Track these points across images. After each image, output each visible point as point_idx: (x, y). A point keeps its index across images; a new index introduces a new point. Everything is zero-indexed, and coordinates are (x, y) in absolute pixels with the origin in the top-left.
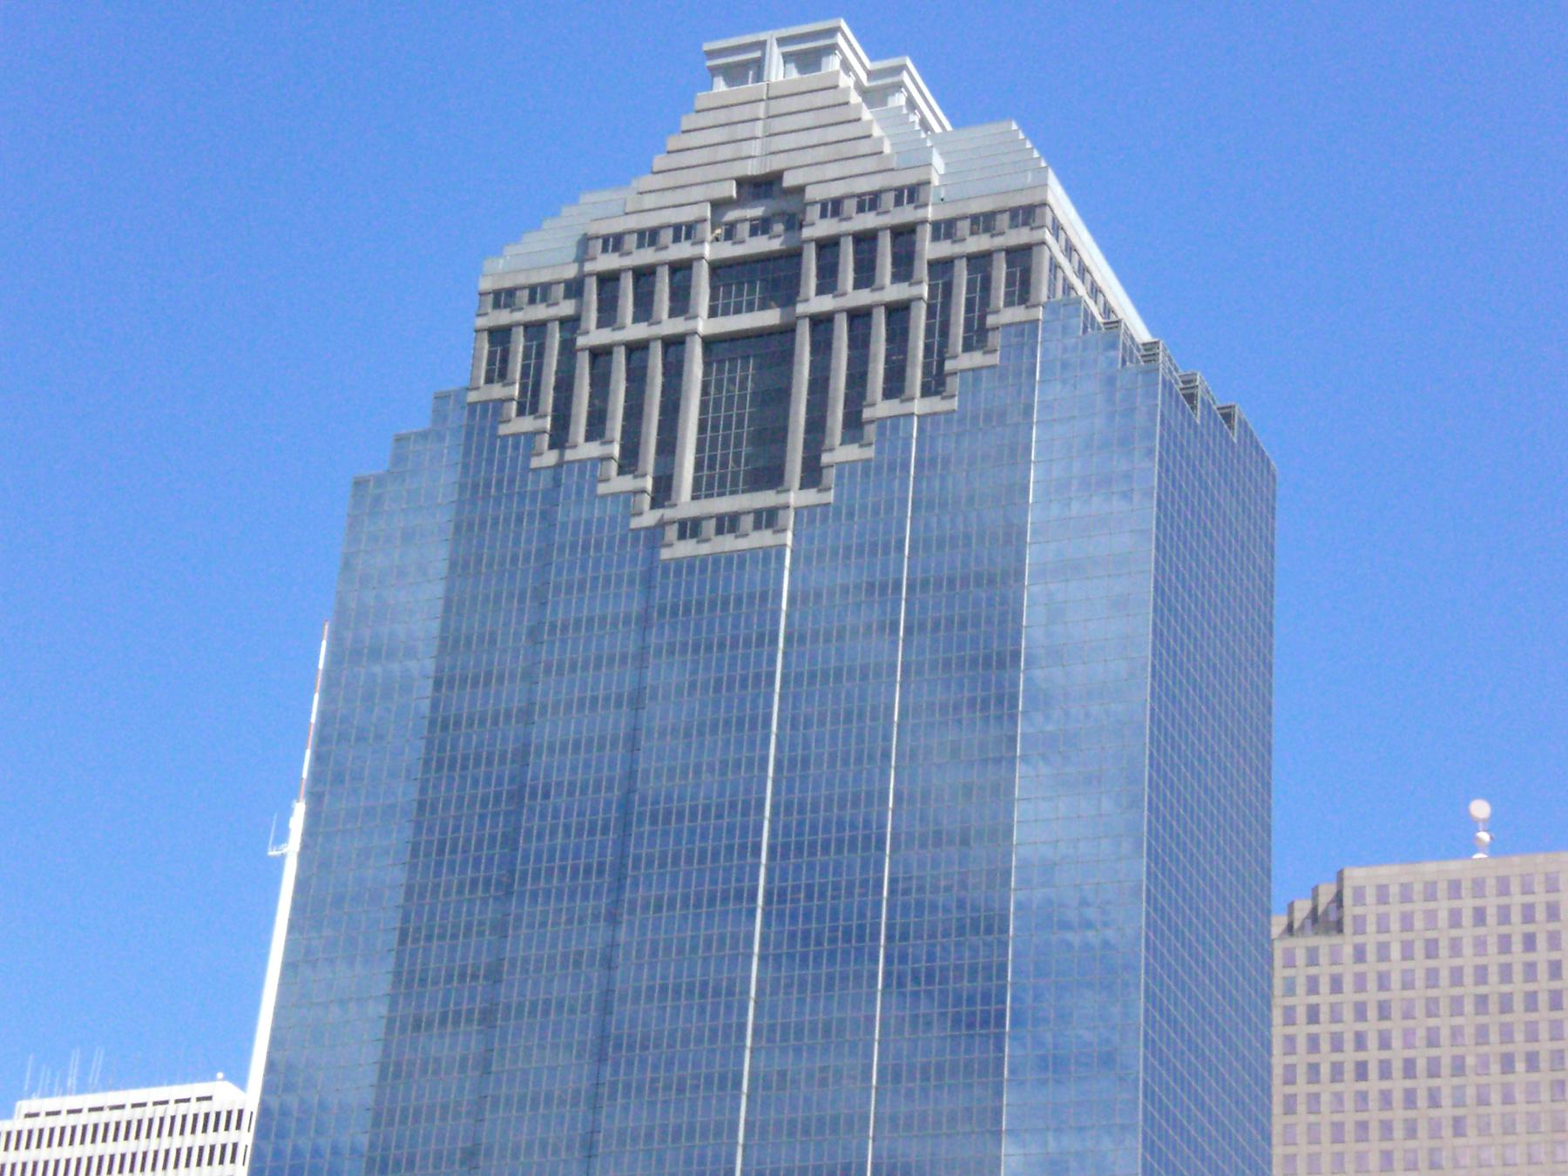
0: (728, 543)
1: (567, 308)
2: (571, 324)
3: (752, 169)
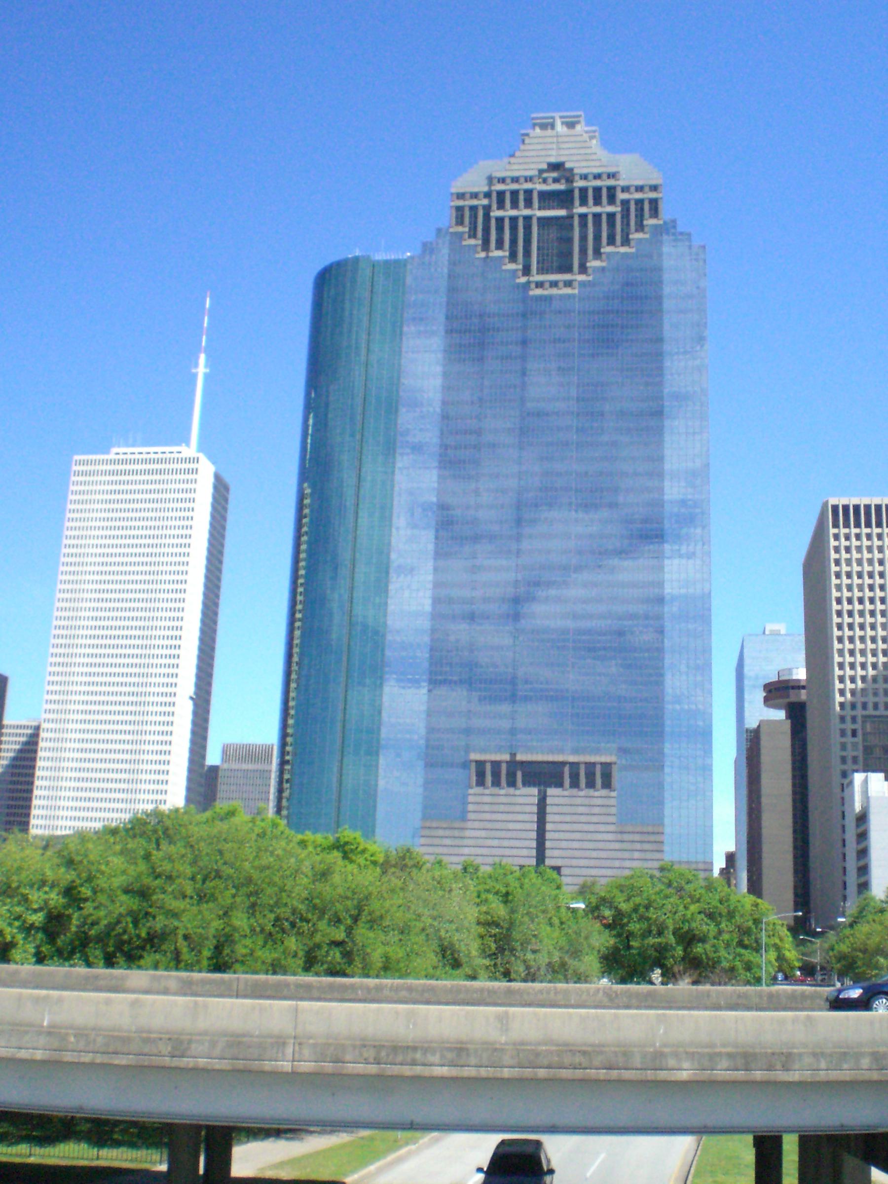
0: (554, 291)
1: (485, 202)
2: (487, 209)
3: (553, 160)
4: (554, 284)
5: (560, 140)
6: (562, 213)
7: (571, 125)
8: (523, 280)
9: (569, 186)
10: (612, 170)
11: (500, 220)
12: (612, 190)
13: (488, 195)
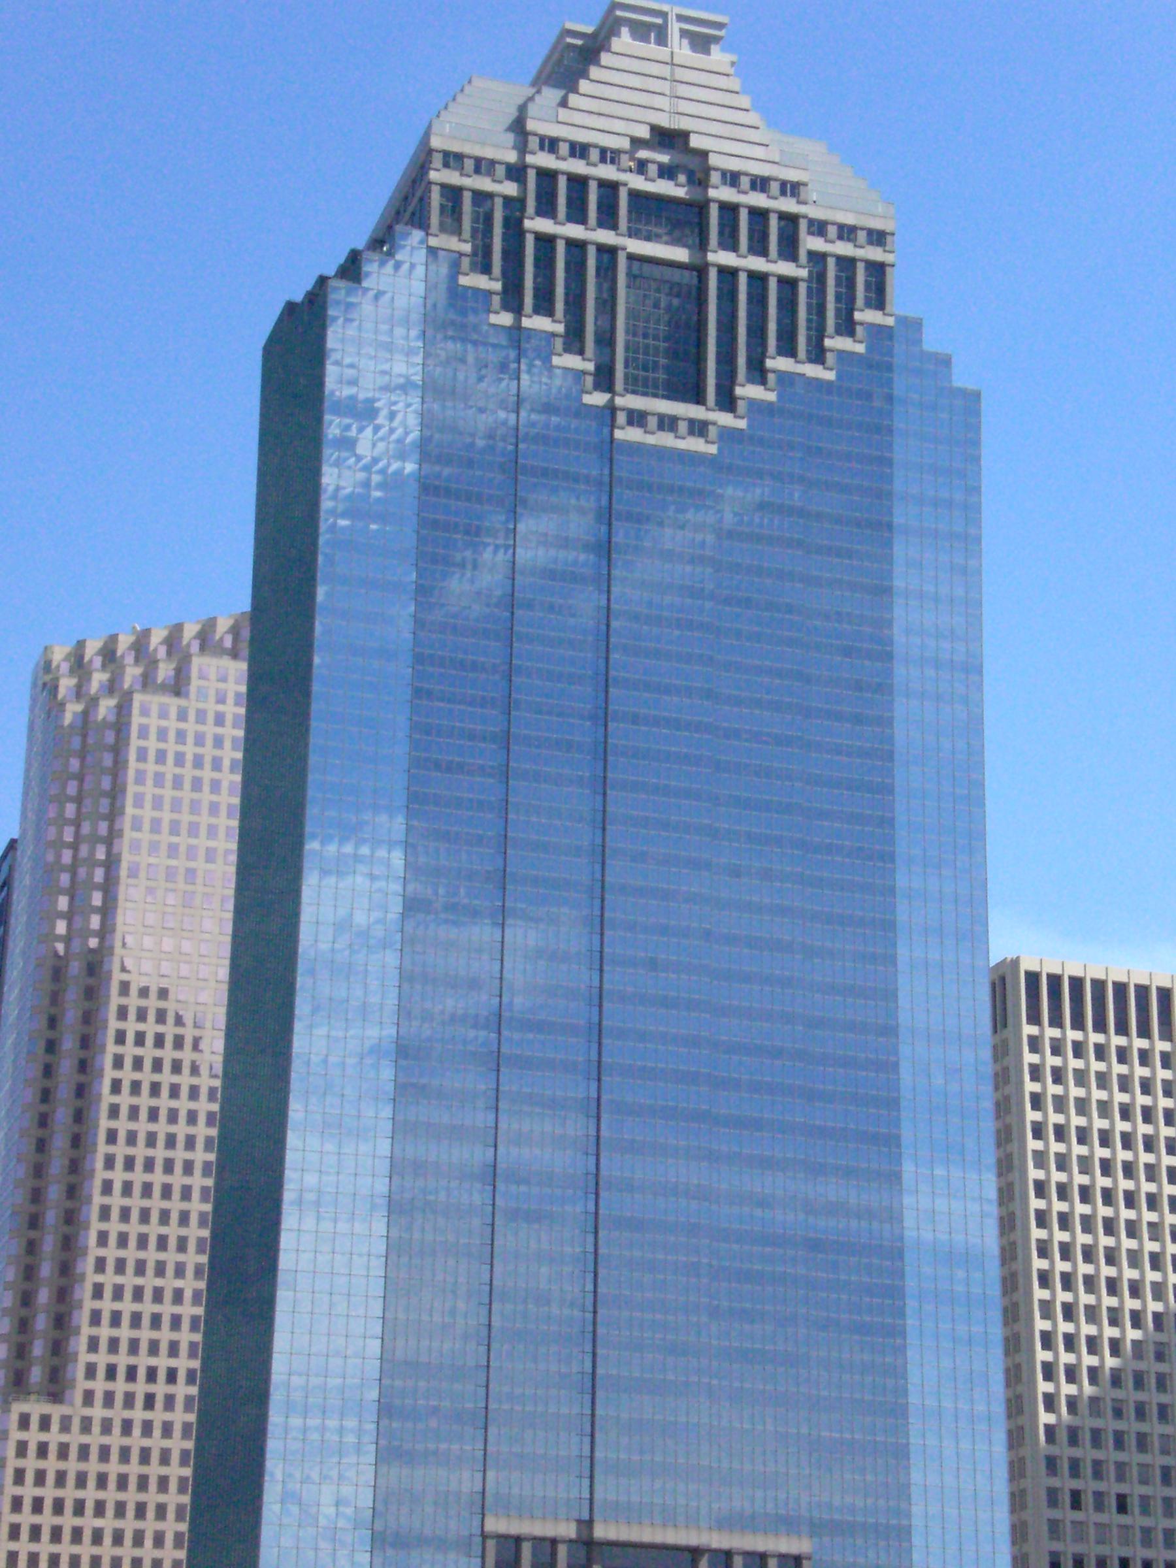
0: (666, 440)
1: (510, 189)
2: (514, 205)
3: (664, 121)
4: (668, 423)
5: (681, 74)
6: (680, 254)
7: (701, 43)
8: (598, 399)
9: (697, 195)
10: (792, 175)
11: (546, 242)
12: (790, 220)
13: (516, 172)
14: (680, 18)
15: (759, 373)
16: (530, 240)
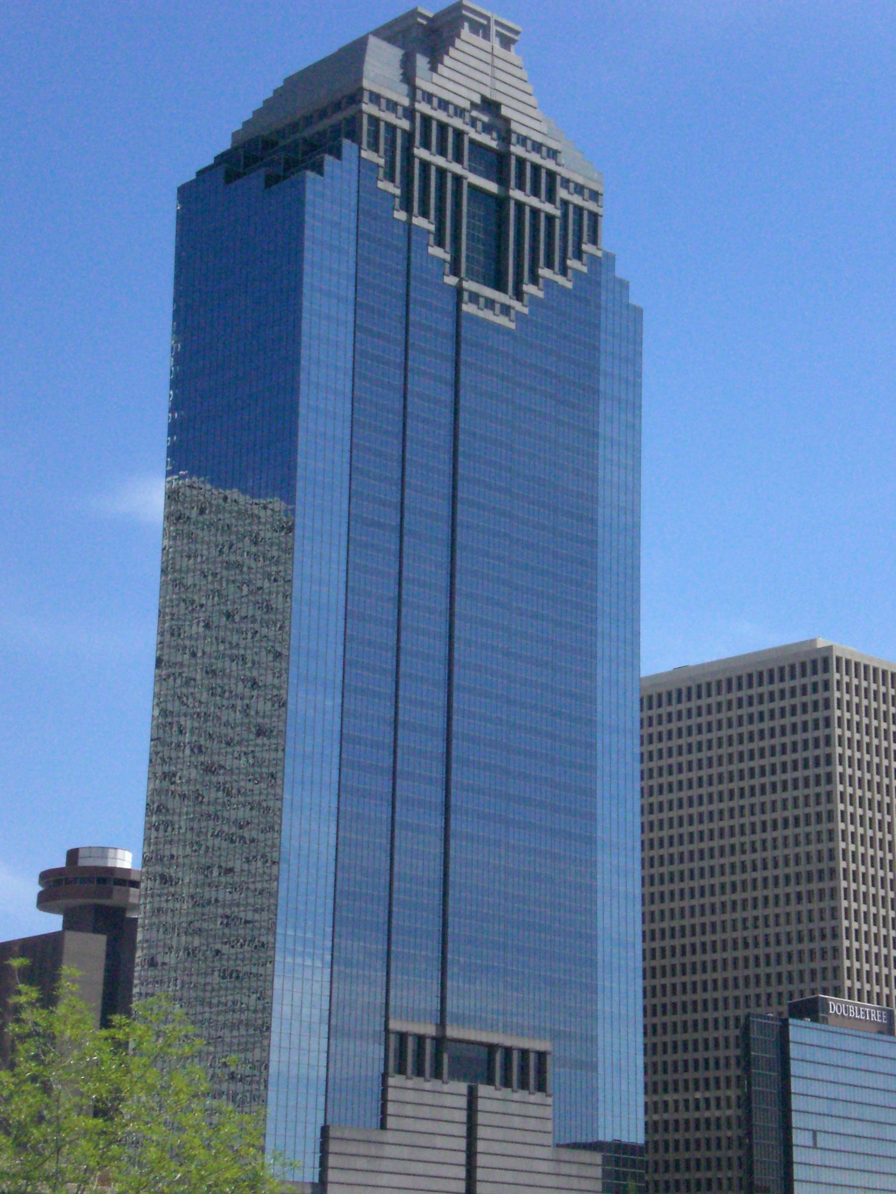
3: (487, 93)
4: (490, 304)
8: (451, 280)
10: (554, 145)
12: (551, 175)
14: (497, 23)
15: (535, 279)
16: (417, 161)
